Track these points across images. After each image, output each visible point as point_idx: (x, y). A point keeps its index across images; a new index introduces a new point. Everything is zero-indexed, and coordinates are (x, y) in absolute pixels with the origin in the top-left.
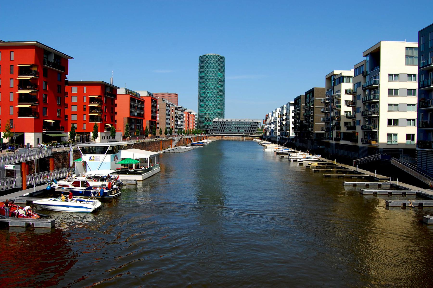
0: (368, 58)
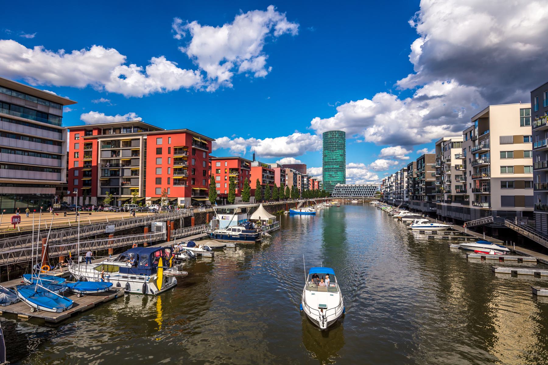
0: (477, 123)
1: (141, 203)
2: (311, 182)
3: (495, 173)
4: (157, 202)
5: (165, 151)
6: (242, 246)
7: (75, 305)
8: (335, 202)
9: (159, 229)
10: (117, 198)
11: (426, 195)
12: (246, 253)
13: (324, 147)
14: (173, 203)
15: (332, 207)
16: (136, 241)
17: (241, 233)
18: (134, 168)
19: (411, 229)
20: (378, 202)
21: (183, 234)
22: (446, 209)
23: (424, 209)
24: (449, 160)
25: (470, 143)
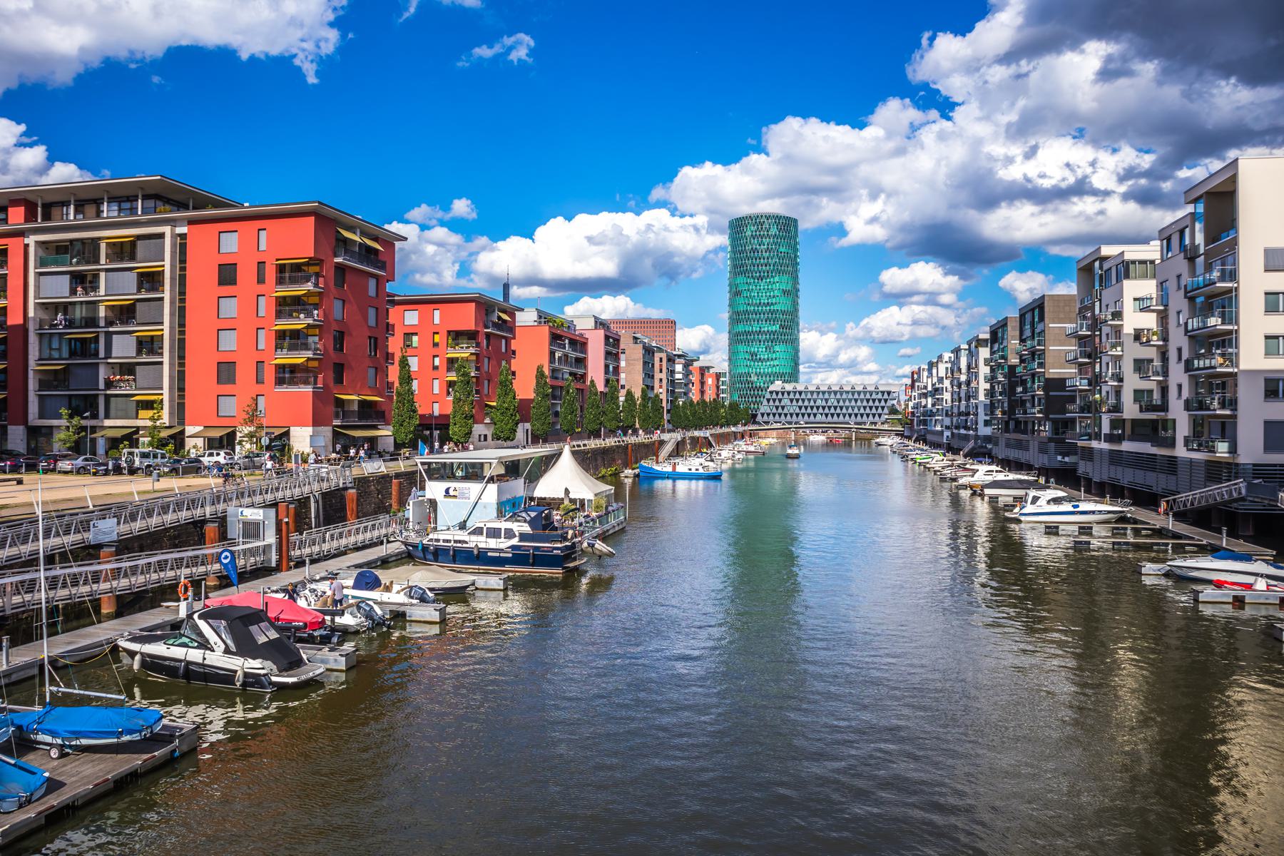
0: (1201, 208)
1: (171, 447)
2: (695, 378)
3: (1252, 356)
4: (227, 442)
5: (246, 275)
6: (517, 585)
7: (53, 785)
8: (768, 441)
9: (252, 530)
10: (94, 429)
11: (1047, 418)
12: (537, 607)
13: (734, 266)
14: (280, 445)
15: (762, 456)
16: (188, 571)
17: (515, 541)
18: (146, 331)
19: (1018, 521)
20: (897, 439)
21: (326, 547)
22: (1106, 459)
23: (1040, 460)
24: (1118, 315)
25: (1181, 265)
